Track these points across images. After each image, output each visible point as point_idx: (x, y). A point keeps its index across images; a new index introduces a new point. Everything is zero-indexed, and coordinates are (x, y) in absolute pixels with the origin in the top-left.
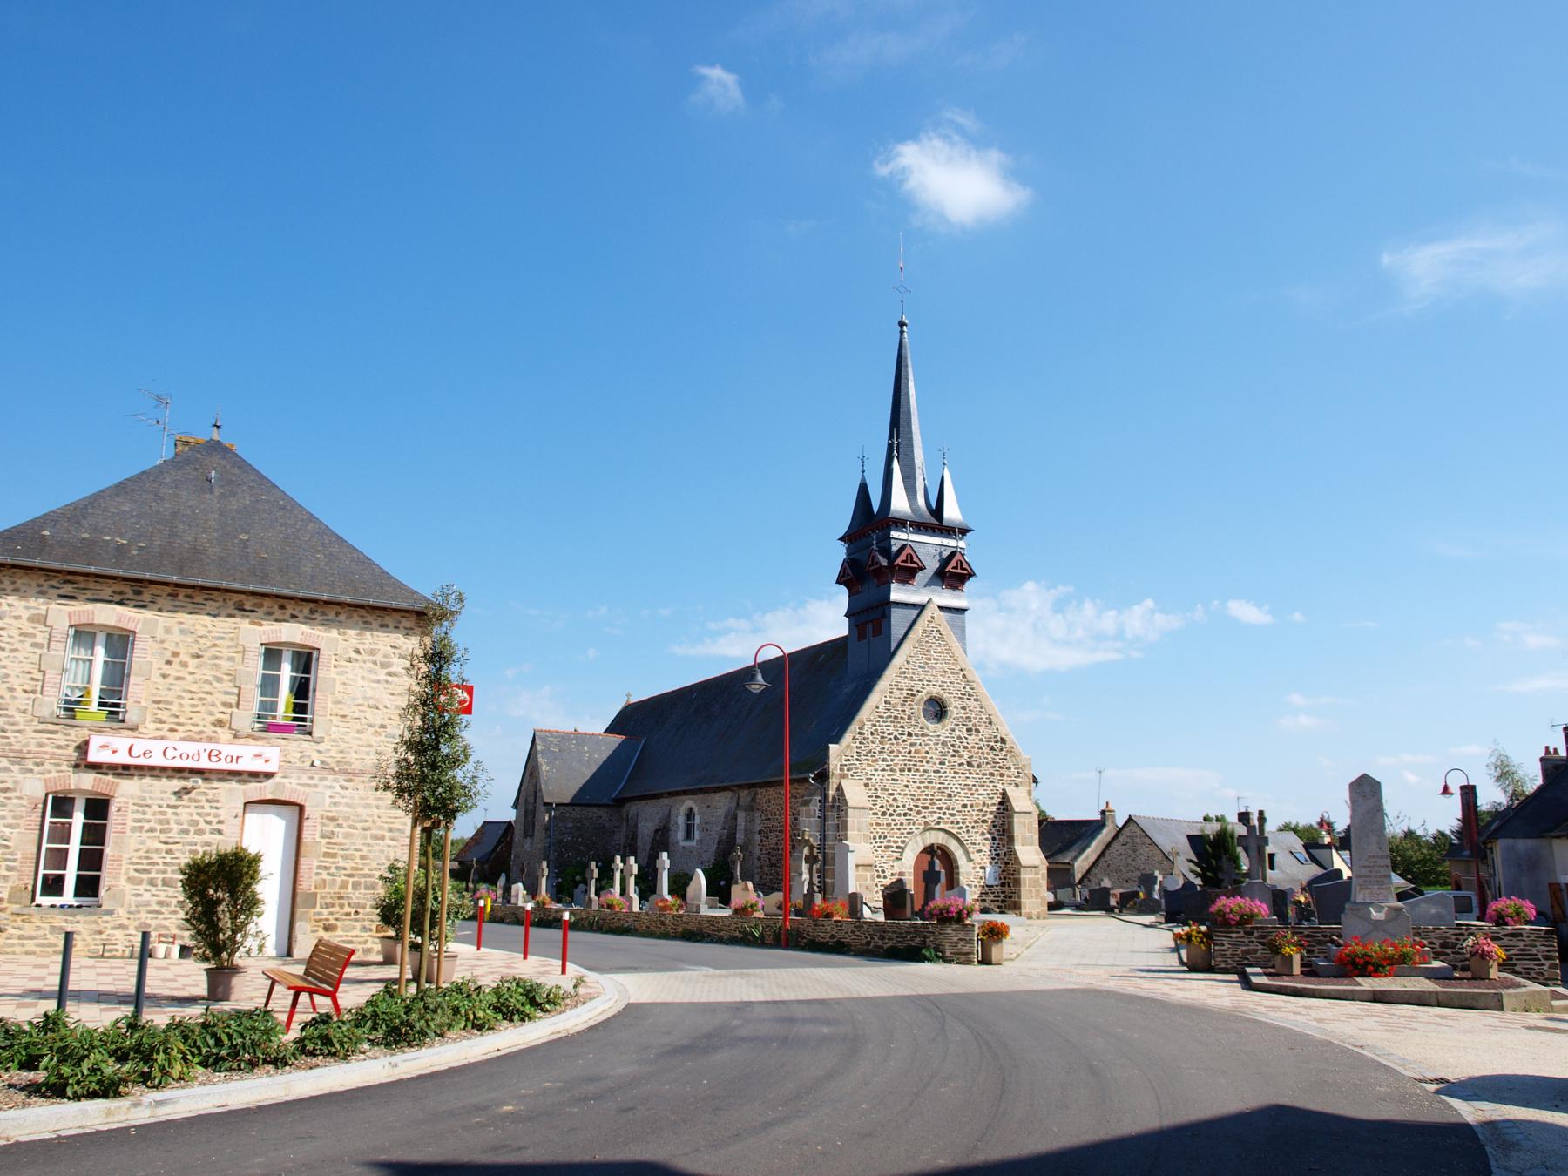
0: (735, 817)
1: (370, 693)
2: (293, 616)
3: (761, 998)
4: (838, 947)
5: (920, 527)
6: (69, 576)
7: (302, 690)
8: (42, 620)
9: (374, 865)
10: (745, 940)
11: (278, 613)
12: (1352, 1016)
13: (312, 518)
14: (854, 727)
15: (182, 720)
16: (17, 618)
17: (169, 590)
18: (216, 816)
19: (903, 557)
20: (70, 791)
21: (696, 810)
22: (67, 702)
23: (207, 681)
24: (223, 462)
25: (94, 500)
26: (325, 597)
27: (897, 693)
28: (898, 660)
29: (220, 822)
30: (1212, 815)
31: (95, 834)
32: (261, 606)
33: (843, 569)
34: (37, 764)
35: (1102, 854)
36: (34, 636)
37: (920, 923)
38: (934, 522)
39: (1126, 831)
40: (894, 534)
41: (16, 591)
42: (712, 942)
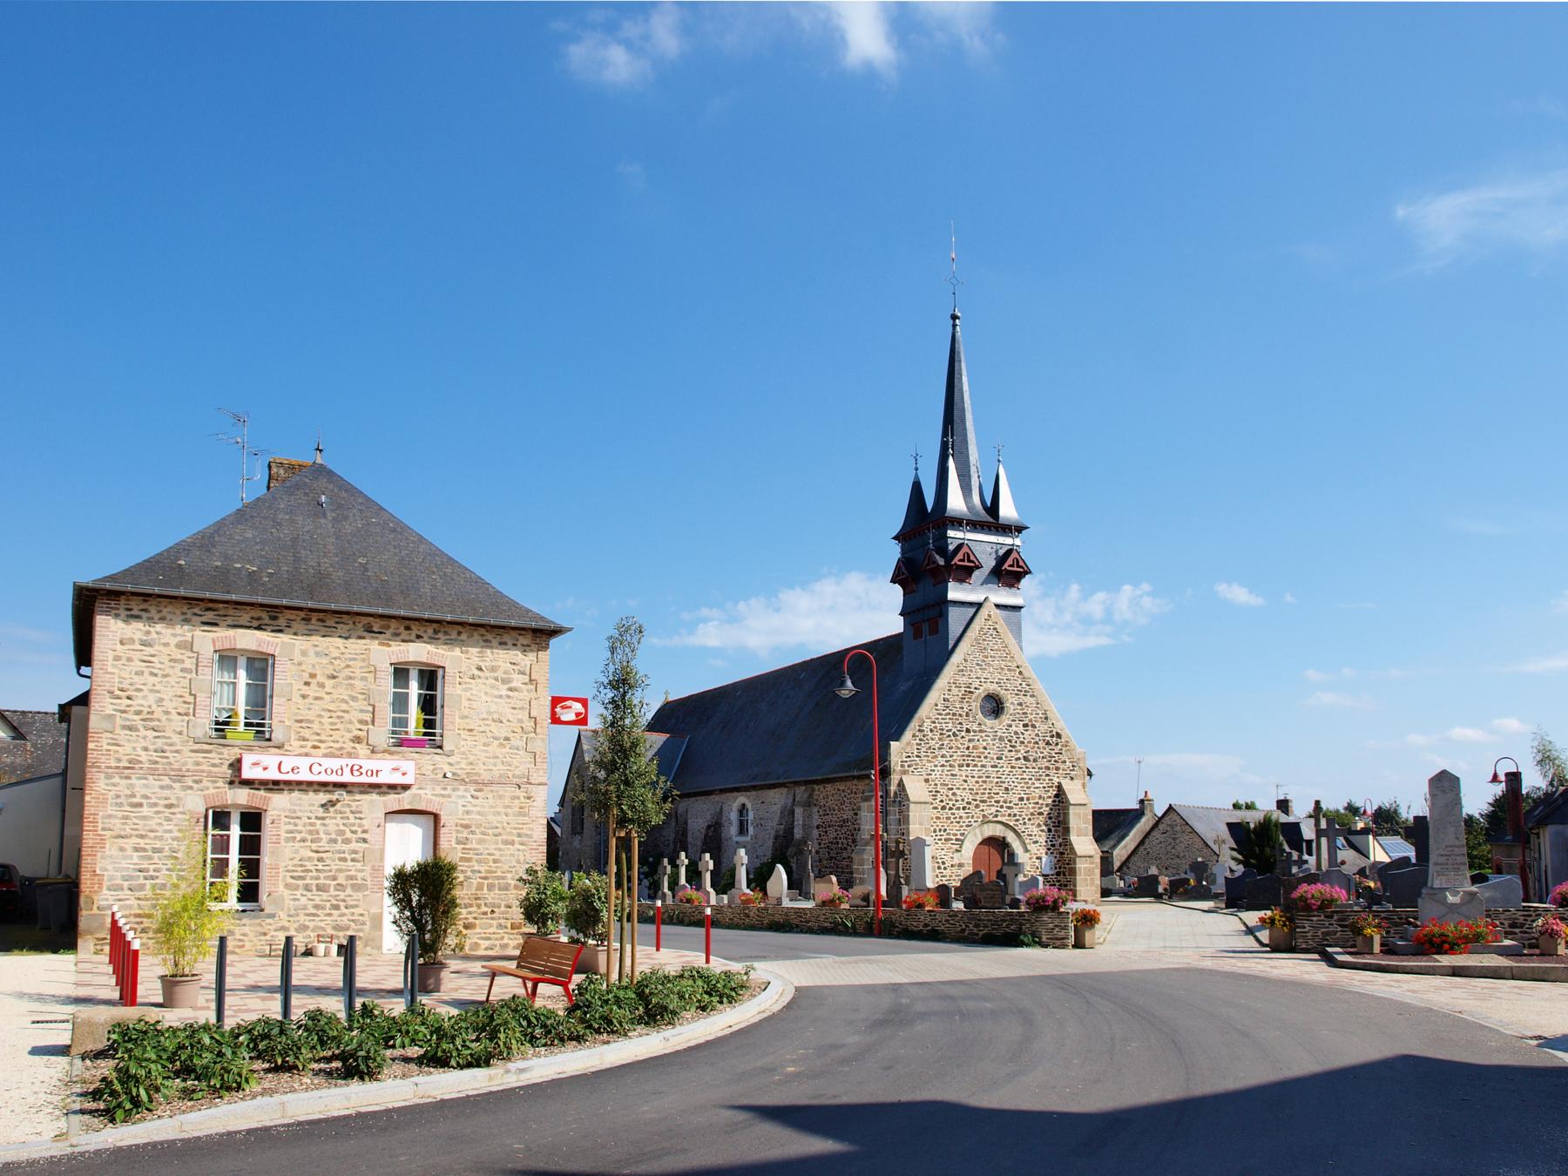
0: (792, 812)
1: (494, 708)
2: (419, 637)
3: (905, 980)
4: (932, 935)
5: (976, 525)
6: (210, 604)
7: (428, 705)
8: (189, 646)
9: (506, 868)
10: (837, 929)
11: (405, 634)
12: (1440, 988)
13: (421, 540)
14: (914, 725)
15: (323, 737)
16: (166, 645)
17: (302, 614)
18: (360, 826)
19: (960, 556)
20: (227, 806)
21: (749, 806)
22: (217, 723)
23: (343, 701)
24: (331, 486)
25: (220, 526)
26: (449, 618)
27: (955, 690)
28: (956, 658)
29: (364, 832)
30: (1242, 802)
31: (251, 846)
32: (388, 627)
33: (898, 568)
34: (196, 782)
35: (1142, 843)
36: (183, 661)
37: (994, 910)
38: (990, 520)
39: (1167, 820)
40: (951, 533)
41: (162, 619)
42: (801, 932)
